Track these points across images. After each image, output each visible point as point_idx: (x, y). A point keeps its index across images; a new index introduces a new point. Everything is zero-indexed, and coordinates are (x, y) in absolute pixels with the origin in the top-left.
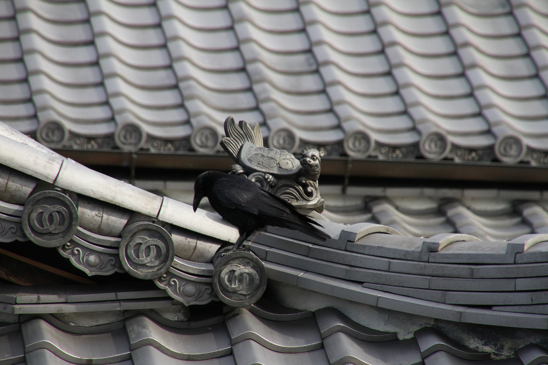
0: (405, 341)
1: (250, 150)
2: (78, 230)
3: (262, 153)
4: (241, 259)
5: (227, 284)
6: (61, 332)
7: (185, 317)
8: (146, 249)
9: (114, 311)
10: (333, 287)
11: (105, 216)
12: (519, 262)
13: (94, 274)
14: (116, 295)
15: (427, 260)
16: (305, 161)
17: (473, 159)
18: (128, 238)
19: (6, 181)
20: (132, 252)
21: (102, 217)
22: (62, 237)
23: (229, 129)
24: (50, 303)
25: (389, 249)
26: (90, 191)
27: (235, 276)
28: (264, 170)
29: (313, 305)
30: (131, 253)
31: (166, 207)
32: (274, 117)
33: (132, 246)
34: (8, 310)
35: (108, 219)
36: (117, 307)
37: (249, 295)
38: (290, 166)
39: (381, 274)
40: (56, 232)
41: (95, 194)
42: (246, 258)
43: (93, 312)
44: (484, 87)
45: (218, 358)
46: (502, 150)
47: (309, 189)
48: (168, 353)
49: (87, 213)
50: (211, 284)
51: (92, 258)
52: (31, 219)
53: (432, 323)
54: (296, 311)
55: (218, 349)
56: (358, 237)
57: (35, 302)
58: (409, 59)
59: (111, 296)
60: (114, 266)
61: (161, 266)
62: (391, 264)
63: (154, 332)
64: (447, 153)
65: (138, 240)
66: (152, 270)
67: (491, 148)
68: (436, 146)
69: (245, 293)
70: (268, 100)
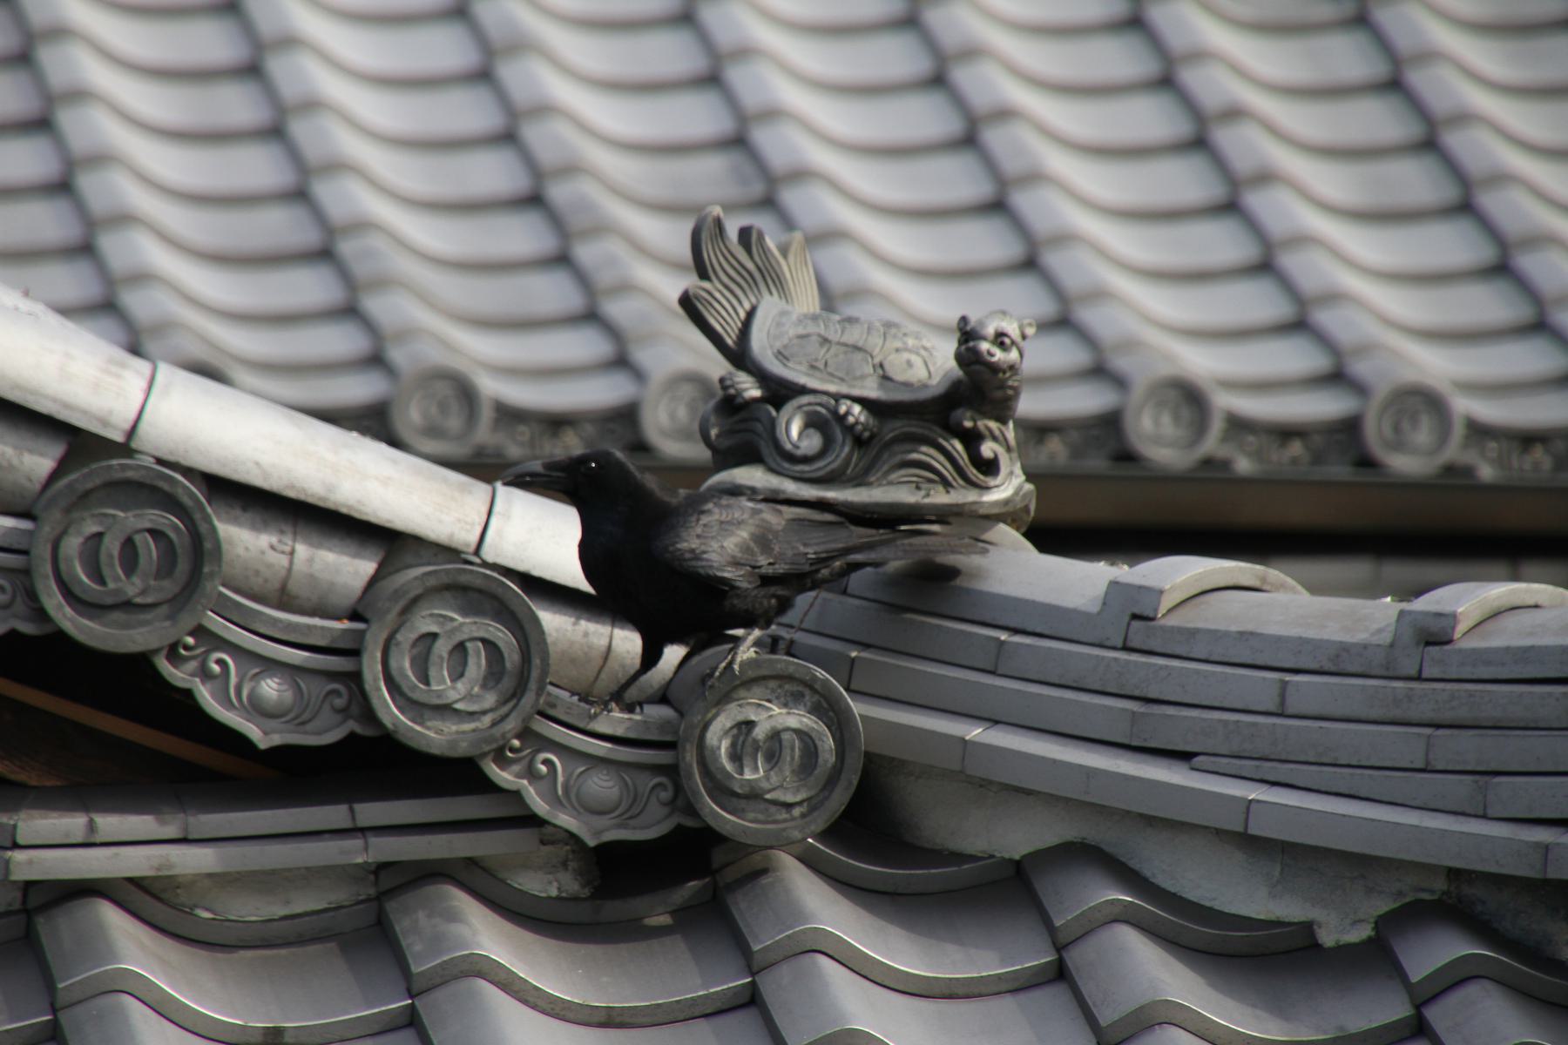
0: (1344, 950)
1: (779, 324)
2: (221, 594)
4: (772, 684)
5: (729, 767)
6: (168, 943)
7: (583, 886)
8: (451, 653)
9: (343, 867)
10: (1090, 773)
11: (302, 550)
13: (276, 740)
14: (352, 810)
15: (1413, 672)
16: (976, 352)
17: (1294, 461)
18: (392, 616)
20: (403, 664)
21: (292, 553)
23: (708, 252)
24: (129, 841)
27: (755, 741)
28: (832, 388)
29: (1016, 836)
30: (401, 669)
31: (507, 516)
33: (406, 646)
35: (311, 561)
36: (355, 852)
37: (800, 803)
38: (918, 373)
39: (1255, 724)
40: (149, 600)
42: (790, 678)
43: (273, 872)
45: (706, 1016)
46: (1388, 431)
47: (987, 449)
48: (539, 1002)
49: (246, 542)
50: (672, 771)
51: (271, 688)
53: (1440, 885)
54: (958, 858)
55: (705, 986)
56: (1166, 603)
57: (80, 840)
58: (1059, 163)
59: (333, 815)
60: (344, 712)
61: (505, 709)
63: (486, 935)
64: (1212, 444)
65: (424, 623)
67: (1350, 427)
69: (790, 799)
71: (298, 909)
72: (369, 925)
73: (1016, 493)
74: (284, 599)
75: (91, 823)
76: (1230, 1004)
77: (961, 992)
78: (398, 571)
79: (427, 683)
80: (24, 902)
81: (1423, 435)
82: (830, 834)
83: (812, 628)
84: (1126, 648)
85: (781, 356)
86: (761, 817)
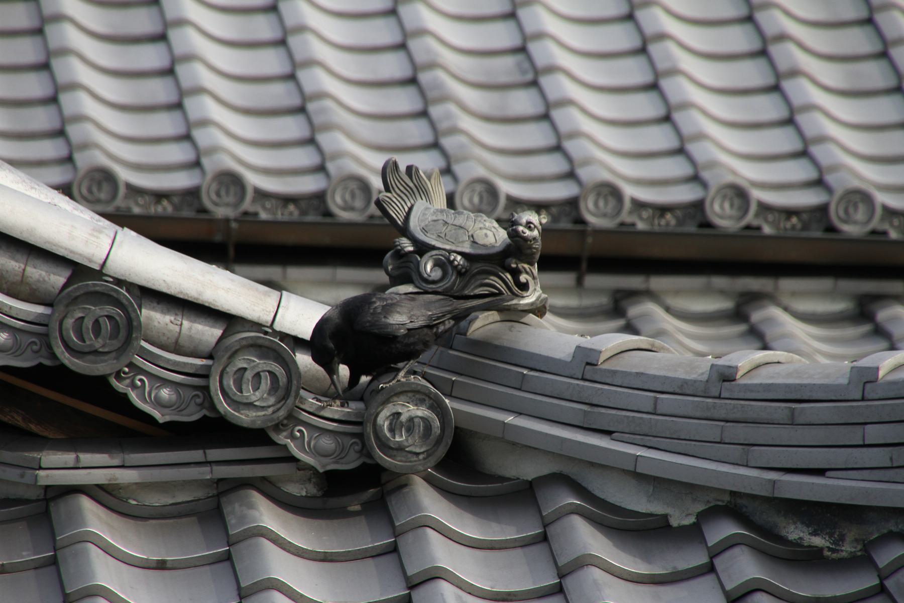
1: (424, 214)
2: (142, 347)
3: (445, 218)
4: (410, 395)
5: (388, 435)
6: (114, 516)
7: (318, 491)
8: (253, 377)
9: (201, 480)
10: (563, 440)
11: (186, 324)
12: (870, 398)
13: (168, 418)
14: (205, 453)
15: (717, 394)
16: (516, 231)
17: (793, 227)
18: (224, 359)
19: (23, 266)
20: (230, 383)
21: (181, 325)
22: (116, 358)
23: (390, 178)
24: (96, 467)
25: (655, 377)
26: (161, 282)
27: (401, 422)
28: (448, 247)
30: (229, 385)
31: (287, 308)
32: (464, 159)
33: (231, 374)
34: (28, 479)
35: (190, 329)
36: (205, 473)
37: (423, 453)
38: (490, 240)
39: (641, 418)
40: (106, 350)
41: (169, 287)
42: (418, 392)
43: (166, 482)
44: (811, 107)
45: (372, 557)
46: (841, 213)
47: (523, 278)
48: (292, 549)
49: (156, 319)
50: (360, 436)
51: (165, 393)
52: (64, 328)
53: (727, 498)
54: (502, 479)
58: (687, 63)
59: (196, 455)
60: (201, 405)
62: (659, 402)
63: (267, 515)
66: (263, 413)
67: (823, 209)
68: (732, 206)
69: (418, 450)
70: (454, 130)
71: (180, 500)
72: (210, 510)
73: (537, 299)
74: (176, 348)
75: (77, 457)
76: (623, 555)
77: (497, 546)
78: (233, 334)
79: (241, 392)
80: (45, 495)
81: (860, 215)
82: (439, 467)
83: (435, 365)
84: (583, 379)
85: (424, 230)
86: (403, 459)
